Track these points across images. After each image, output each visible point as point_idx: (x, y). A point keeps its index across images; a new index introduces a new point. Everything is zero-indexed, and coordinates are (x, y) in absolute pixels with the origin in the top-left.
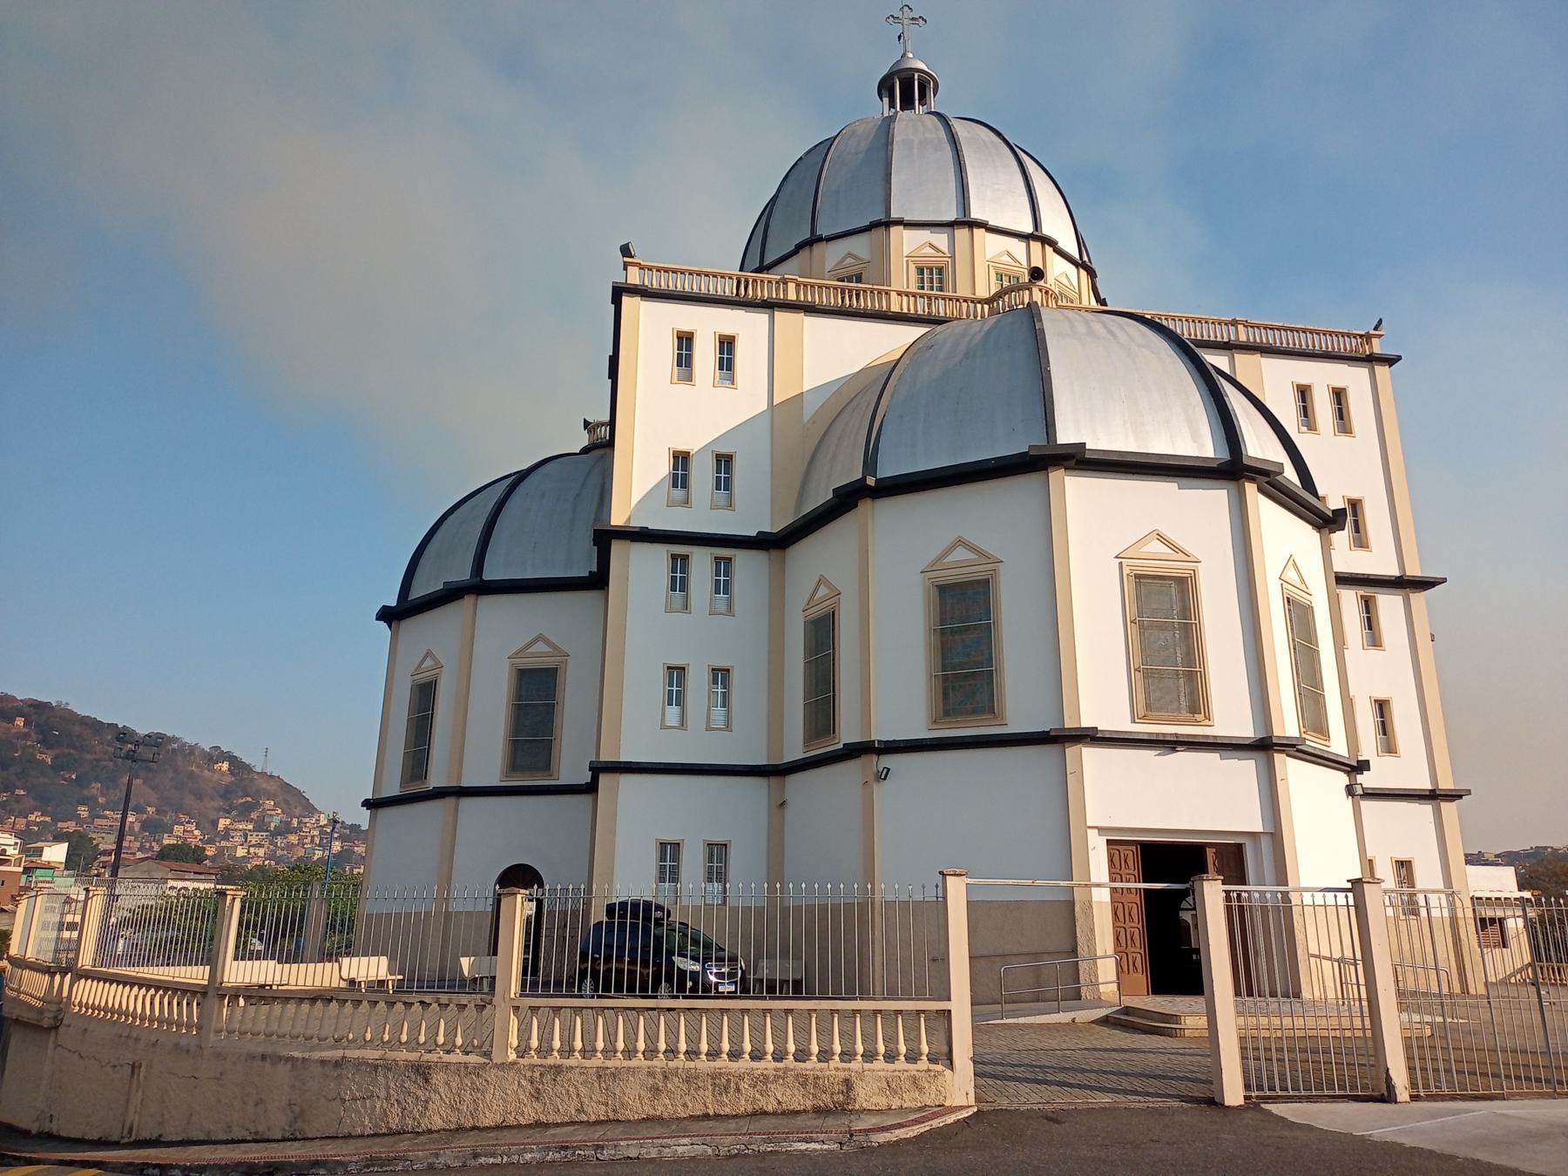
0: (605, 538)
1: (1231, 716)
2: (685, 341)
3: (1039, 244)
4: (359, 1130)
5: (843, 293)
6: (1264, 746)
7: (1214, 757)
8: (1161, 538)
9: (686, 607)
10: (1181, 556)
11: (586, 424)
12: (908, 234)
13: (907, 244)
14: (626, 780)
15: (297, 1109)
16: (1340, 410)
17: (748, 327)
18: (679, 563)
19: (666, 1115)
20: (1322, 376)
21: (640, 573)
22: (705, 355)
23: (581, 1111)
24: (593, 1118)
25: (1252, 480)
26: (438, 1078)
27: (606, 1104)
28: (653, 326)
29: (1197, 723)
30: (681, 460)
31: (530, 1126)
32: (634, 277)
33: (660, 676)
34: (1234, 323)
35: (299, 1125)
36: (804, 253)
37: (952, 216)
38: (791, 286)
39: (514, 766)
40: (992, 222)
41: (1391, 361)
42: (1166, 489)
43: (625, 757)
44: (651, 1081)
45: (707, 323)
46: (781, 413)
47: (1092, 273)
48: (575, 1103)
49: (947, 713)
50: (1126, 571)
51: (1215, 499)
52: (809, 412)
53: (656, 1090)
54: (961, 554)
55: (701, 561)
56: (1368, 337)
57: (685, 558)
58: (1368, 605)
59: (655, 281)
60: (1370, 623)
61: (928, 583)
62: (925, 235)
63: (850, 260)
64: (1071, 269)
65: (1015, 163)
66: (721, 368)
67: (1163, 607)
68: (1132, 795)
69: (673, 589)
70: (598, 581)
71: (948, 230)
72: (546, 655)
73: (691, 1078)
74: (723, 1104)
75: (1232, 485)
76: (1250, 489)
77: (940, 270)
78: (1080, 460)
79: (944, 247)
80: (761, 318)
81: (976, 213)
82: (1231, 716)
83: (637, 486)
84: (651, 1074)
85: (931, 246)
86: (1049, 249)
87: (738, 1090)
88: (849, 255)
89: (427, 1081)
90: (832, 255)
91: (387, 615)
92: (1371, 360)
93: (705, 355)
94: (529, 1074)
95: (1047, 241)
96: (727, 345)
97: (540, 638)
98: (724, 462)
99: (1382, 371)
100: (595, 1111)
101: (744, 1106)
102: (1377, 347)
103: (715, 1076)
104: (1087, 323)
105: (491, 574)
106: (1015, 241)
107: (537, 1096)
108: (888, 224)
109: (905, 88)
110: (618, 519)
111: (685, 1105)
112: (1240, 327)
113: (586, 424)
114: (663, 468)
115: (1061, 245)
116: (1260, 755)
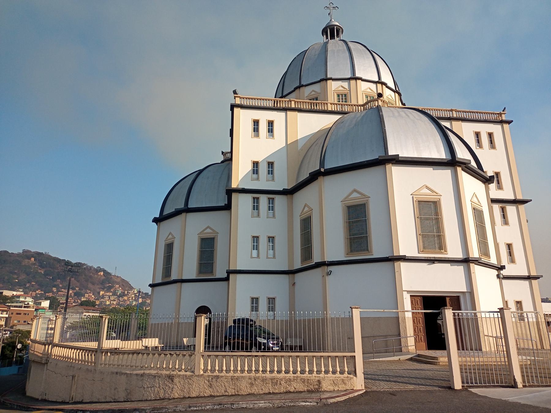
0: (230, 192)
1: (454, 250)
2: (256, 123)
3: (380, 85)
4: (150, 398)
5: (311, 104)
6: (466, 261)
7: (448, 265)
8: (427, 188)
9: (258, 215)
10: (435, 194)
11: (223, 153)
12: (333, 83)
13: (333, 86)
14: (239, 276)
15: (129, 391)
16: (478, 140)
17: (278, 117)
18: (256, 200)
19: (255, 393)
20: (484, 129)
21: (242, 204)
22: (263, 127)
23: (226, 391)
24: (230, 394)
25: (460, 166)
26: (176, 380)
27: (235, 389)
28: (244, 118)
29: (442, 253)
30: (256, 164)
31: (208, 397)
32: (238, 101)
33: (250, 239)
34: (452, 110)
35: (129, 397)
36: (297, 91)
37: (349, 76)
38: (293, 103)
39: (200, 272)
40: (364, 78)
41: (509, 122)
42: (428, 170)
43: (238, 268)
44: (250, 381)
45: (264, 116)
46: (290, 147)
47: (400, 95)
48: (223, 389)
49: (351, 251)
50: (415, 199)
51: (447, 173)
52: (300, 146)
53: (252, 384)
54: (355, 195)
55: (263, 199)
56: (500, 114)
57: (258, 198)
58: (503, 210)
59: (245, 103)
60: (504, 216)
61: (344, 205)
62: (340, 83)
63: (313, 93)
64: (392, 93)
65: (371, 57)
66: (269, 132)
67: (428, 212)
68: (418, 279)
69: (254, 209)
70: (228, 207)
71: (348, 81)
72: (211, 233)
73: (264, 380)
74: (275, 389)
75: (452, 168)
76: (459, 169)
77: (345, 95)
78: (397, 161)
79: (347, 87)
80: (283, 114)
81: (358, 75)
82: (454, 250)
83: (240, 174)
84: (250, 379)
85: (342, 87)
86: (384, 86)
87: (280, 384)
88: (313, 91)
89: (173, 381)
90: (307, 91)
91: (156, 220)
92: (502, 122)
93: (263, 127)
94: (208, 379)
95: (383, 84)
96: (271, 124)
97: (208, 227)
98: (271, 164)
99: (506, 126)
100: (231, 391)
101: (282, 390)
102: (504, 118)
103: (272, 379)
104: (399, 112)
105: (191, 205)
106: (372, 84)
107: (211, 386)
108: (327, 79)
109: (331, 32)
110: (234, 185)
111: (262, 389)
112: (454, 112)
113: (223, 153)
114: (250, 167)
115: (389, 85)
116: (465, 264)
